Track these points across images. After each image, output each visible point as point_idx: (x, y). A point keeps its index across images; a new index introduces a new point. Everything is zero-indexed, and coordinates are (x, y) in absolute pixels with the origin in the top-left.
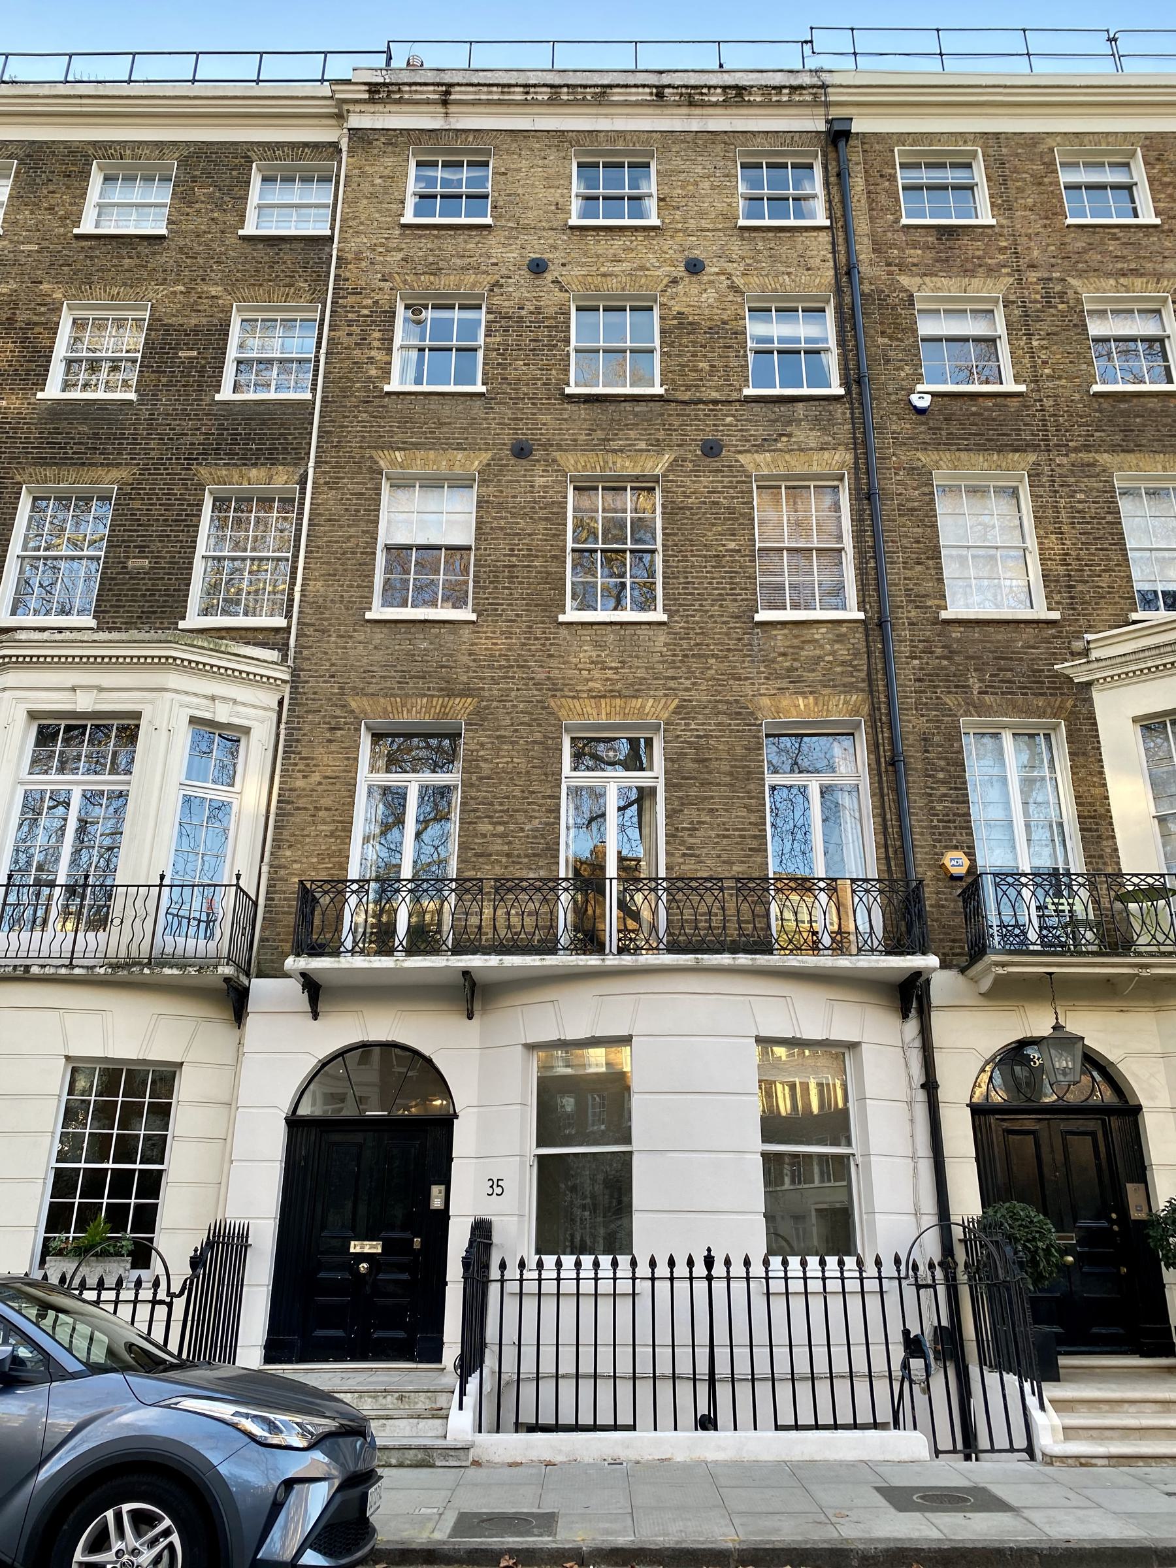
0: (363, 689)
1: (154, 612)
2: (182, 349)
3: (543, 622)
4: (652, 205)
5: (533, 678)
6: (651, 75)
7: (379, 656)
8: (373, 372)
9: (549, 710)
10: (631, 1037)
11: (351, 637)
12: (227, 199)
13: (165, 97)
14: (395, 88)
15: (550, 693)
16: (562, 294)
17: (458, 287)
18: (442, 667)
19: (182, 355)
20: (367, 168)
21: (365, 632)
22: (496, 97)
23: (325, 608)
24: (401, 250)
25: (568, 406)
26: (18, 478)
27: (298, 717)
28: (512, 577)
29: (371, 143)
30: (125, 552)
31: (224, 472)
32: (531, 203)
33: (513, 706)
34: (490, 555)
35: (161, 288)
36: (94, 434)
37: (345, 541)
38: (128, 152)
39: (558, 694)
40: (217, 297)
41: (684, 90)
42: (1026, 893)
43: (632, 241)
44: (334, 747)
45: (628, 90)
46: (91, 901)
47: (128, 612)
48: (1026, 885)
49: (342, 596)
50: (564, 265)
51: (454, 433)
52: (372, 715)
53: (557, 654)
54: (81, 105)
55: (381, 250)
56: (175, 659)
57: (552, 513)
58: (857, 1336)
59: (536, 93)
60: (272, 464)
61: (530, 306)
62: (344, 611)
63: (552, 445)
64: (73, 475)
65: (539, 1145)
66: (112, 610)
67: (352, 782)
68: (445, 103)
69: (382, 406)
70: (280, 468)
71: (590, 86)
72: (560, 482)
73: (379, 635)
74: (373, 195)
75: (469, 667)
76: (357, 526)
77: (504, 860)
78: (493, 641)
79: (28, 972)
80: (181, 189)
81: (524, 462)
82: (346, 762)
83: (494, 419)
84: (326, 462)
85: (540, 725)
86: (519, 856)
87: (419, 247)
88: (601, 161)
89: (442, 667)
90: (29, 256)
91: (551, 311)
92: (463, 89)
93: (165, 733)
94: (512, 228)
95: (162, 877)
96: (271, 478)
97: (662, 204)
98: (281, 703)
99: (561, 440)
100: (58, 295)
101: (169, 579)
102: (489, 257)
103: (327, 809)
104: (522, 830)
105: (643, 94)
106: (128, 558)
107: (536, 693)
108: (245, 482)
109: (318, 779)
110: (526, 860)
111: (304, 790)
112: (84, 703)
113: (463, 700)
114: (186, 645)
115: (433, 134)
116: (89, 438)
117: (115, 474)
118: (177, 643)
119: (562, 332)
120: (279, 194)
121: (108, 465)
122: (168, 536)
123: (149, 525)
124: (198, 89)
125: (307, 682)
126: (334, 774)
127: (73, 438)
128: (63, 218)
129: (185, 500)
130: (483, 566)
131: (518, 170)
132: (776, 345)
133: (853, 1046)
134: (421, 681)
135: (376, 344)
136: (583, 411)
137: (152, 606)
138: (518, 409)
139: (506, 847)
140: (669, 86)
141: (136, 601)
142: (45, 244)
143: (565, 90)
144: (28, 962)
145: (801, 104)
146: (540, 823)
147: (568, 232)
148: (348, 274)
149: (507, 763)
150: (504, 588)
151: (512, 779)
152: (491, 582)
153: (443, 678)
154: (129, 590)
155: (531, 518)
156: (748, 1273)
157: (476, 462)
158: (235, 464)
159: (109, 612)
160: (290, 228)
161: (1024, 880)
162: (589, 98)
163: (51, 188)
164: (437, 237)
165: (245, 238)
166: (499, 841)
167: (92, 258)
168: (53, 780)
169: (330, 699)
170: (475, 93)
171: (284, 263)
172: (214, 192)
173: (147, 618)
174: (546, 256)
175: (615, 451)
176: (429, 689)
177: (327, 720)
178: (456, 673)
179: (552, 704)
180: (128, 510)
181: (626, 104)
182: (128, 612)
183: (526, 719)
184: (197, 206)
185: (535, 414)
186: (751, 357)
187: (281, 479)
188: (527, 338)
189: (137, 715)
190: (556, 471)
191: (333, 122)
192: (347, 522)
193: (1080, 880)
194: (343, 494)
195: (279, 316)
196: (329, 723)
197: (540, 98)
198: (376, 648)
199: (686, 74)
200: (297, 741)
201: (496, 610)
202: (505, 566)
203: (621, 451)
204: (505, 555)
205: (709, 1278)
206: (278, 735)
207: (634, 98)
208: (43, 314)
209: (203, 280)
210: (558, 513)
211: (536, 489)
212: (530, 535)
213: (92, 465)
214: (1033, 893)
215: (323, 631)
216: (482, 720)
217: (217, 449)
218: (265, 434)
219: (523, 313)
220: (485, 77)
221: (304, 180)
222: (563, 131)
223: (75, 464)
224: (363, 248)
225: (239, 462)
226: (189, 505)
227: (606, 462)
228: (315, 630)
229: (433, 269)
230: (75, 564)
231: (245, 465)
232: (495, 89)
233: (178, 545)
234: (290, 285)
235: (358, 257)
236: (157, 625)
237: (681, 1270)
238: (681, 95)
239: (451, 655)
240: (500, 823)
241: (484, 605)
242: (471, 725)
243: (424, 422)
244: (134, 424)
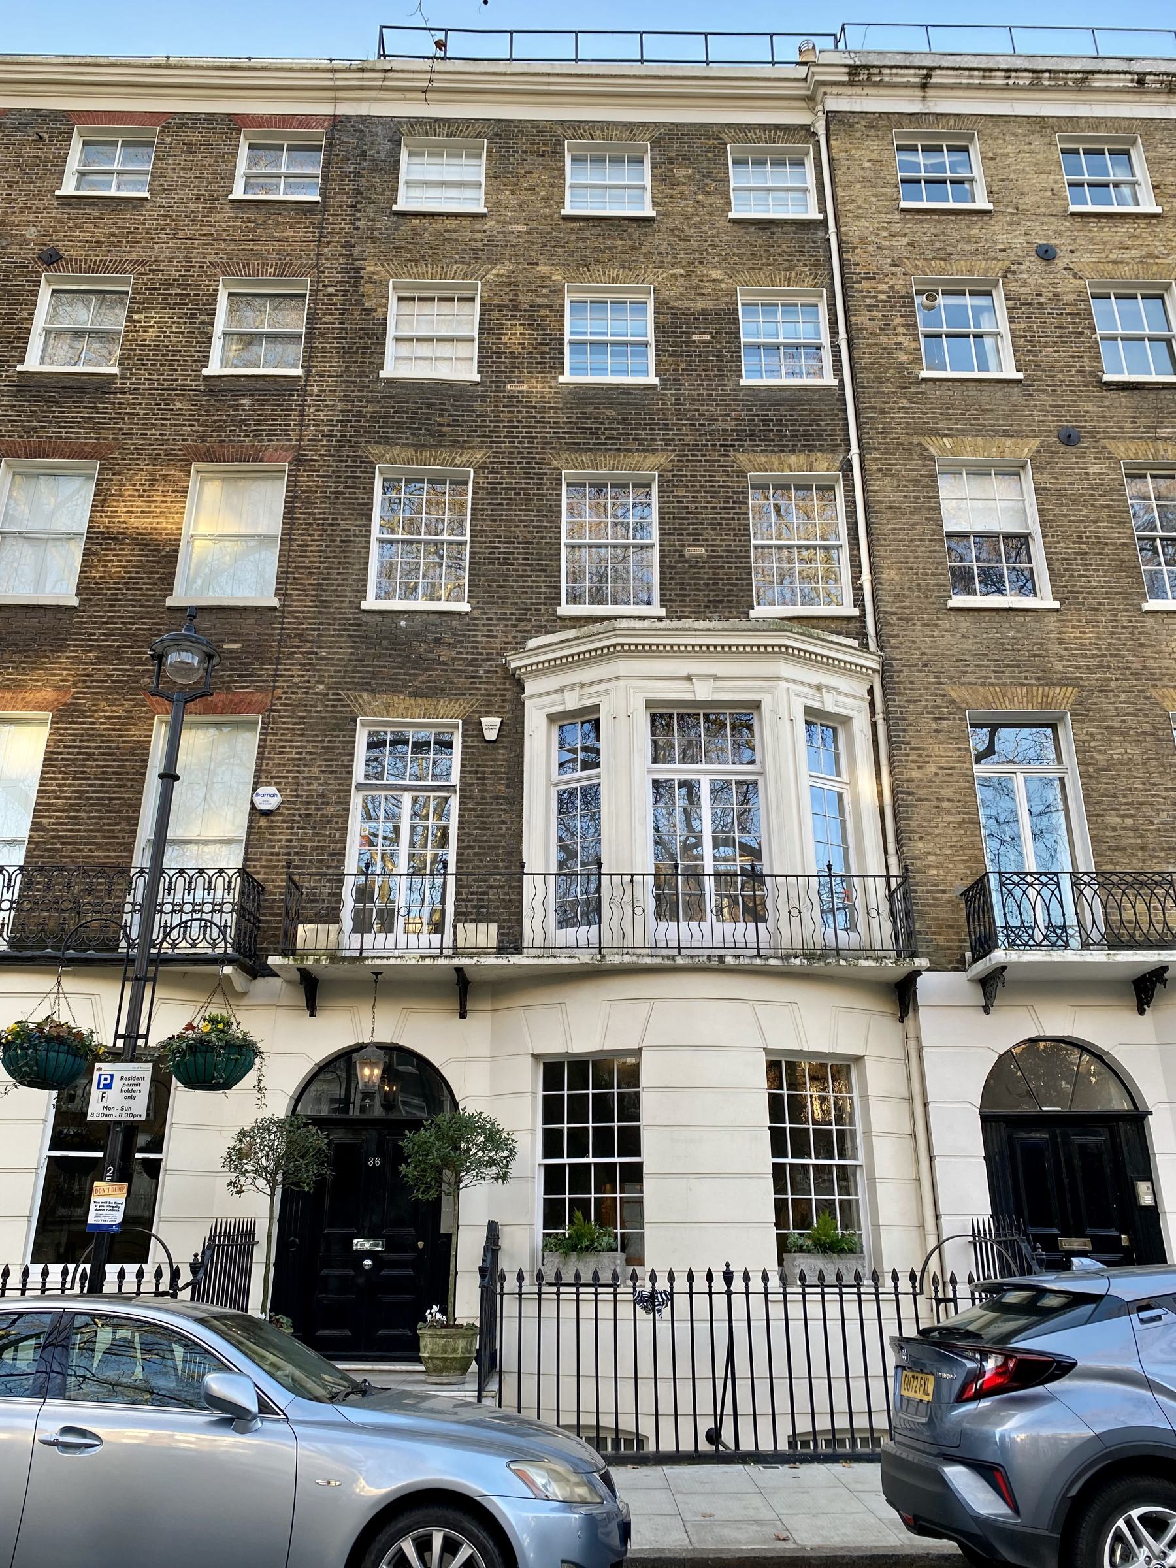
0: (959, 678)
1: (721, 601)
2: (694, 333)
3: (1127, 611)
4: (980, 190)
5: (1129, 668)
6: (1121, 62)
7: (968, 645)
8: (904, 358)
9: (1153, 701)
10: (640, 1049)
11: (936, 626)
12: (708, 181)
13: (635, 77)
14: (876, 71)
15: (1150, 683)
16: (1078, 281)
17: (971, 272)
18: (1035, 655)
19: (698, 339)
20: (853, 152)
21: (950, 620)
22: (977, 81)
23: (904, 595)
24: (905, 234)
25: (1108, 394)
26: (555, 464)
27: (900, 707)
28: (1086, 565)
29: (851, 126)
30: (679, 540)
31: (763, 459)
32: (1026, 189)
33: (1115, 696)
34: (1059, 543)
35: (661, 270)
36: (623, 419)
37: (900, 525)
38: (598, 132)
39: (1158, 683)
40: (719, 281)
41: (1165, 78)
42: (1032, 893)
43: (1135, 229)
44: (942, 737)
45: (1110, 76)
46: (748, 893)
47: (695, 601)
48: (1031, 884)
49: (918, 584)
50: (1072, 251)
51: (997, 420)
52: (974, 705)
53: (1147, 642)
54: (549, 83)
55: (885, 234)
56: (622, 645)
57: (1112, 500)
59: (1017, 78)
60: (810, 451)
61: (1047, 293)
62: (923, 600)
63: (1098, 432)
64: (610, 461)
66: (678, 599)
67: (970, 773)
68: (924, 86)
69: (921, 393)
70: (819, 454)
71: (1072, 72)
72: (1114, 469)
73: (964, 624)
74: (864, 180)
75: (1062, 656)
76: (919, 513)
77: (1140, 853)
78: (1082, 630)
79: (723, 962)
80: (660, 170)
81: (1073, 449)
82: (958, 753)
83: (1035, 406)
84: (875, 449)
85: (1146, 716)
86: (1154, 850)
87: (925, 231)
88: (1081, 147)
89: (1035, 655)
90: (519, 237)
91: (1070, 298)
92: (944, 72)
93: (788, 723)
94: (1012, 214)
95: (830, 867)
96: (811, 464)
97: (1157, 191)
98: (871, 691)
99: (1107, 427)
100: (557, 277)
101: (730, 568)
102: (996, 243)
103: (949, 800)
104: (1152, 823)
105: (1124, 80)
106: (683, 546)
107: (1135, 682)
108: (786, 468)
109: (934, 770)
110: (1162, 854)
111: (921, 780)
112: (703, 692)
113: (1064, 689)
114: (798, 633)
115: (913, 118)
116: (618, 423)
117: (652, 460)
118: (791, 631)
119: (1086, 319)
120: (590, 175)
121: (644, 451)
122: (719, 524)
123: (698, 513)
124: (714, 70)
125: (901, 671)
126: (949, 765)
127: (602, 423)
128: (548, 197)
129: (729, 487)
130: (1055, 554)
131: (1007, 155)
134: (1017, 670)
135: (901, 329)
136: (1123, 398)
137: (717, 595)
138: (1058, 396)
139: (1139, 841)
140: (1150, 73)
141: (700, 590)
142: (533, 224)
143: (1047, 75)
144: (722, 952)
145: (1017, 88)
146: (1169, 816)
147: (1069, 218)
148: (858, 259)
149: (1121, 754)
150: (1080, 576)
151: (1129, 770)
152: (1065, 570)
153: (1037, 667)
154: (690, 579)
155: (1092, 505)
157: (1027, 448)
158: (773, 451)
159: (675, 601)
160: (768, 211)
161: (1029, 879)
162: (1070, 83)
163: (527, 168)
164: (939, 222)
165: (734, 221)
166: (1131, 834)
167: (584, 240)
168: (676, 770)
169: (928, 689)
170: (956, 77)
171: (779, 246)
172: (693, 175)
173: (715, 607)
174: (1053, 242)
175: (1165, 439)
176: (1026, 678)
177: (930, 710)
178: (1049, 662)
179: (1154, 694)
180: (674, 497)
181: (1106, 90)
182: (695, 601)
183: (1131, 710)
184: (680, 188)
185: (1075, 401)
186: (922, 339)
187: (823, 466)
188: (1052, 324)
189: (757, 705)
190: (1109, 458)
191: (803, 104)
192: (908, 510)
193: (1086, 878)
194: (899, 481)
195: (779, 300)
196: (932, 713)
197: (1021, 83)
198: (963, 636)
199: (1155, 62)
200: (904, 731)
201: (1077, 598)
202: (1077, 554)
203: (1170, 439)
204: (1074, 543)
205: (729, 1293)
206: (874, 725)
207: (1115, 85)
208: (545, 296)
209: (701, 263)
210: (1119, 501)
211: (1092, 476)
212: (1095, 522)
213: (628, 450)
214: (1039, 893)
215: (908, 620)
216: (1089, 710)
217: (752, 435)
218: (797, 420)
219: (1042, 300)
220: (955, 61)
221: (594, 160)
222: (1043, 117)
223: (610, 450)
224: (867, 232)
225: (776, 449)
226: (734, 492)
227: (1157, 451)
228: (899, 619)
229: (942, 254)
230: (602, 550)
231: (782, 451)
232: (976, 73)
233: (732, 533)
234: (791, 269)
235: (863, 241)
236: (727, 614)
237: (700, 1284)
238: (1162, 82)
239: (1042, 644)
240: (1128, 816)
241: (1063, 592)
242: (1077, 715)
243: (975, 408)
244: (662, 409)
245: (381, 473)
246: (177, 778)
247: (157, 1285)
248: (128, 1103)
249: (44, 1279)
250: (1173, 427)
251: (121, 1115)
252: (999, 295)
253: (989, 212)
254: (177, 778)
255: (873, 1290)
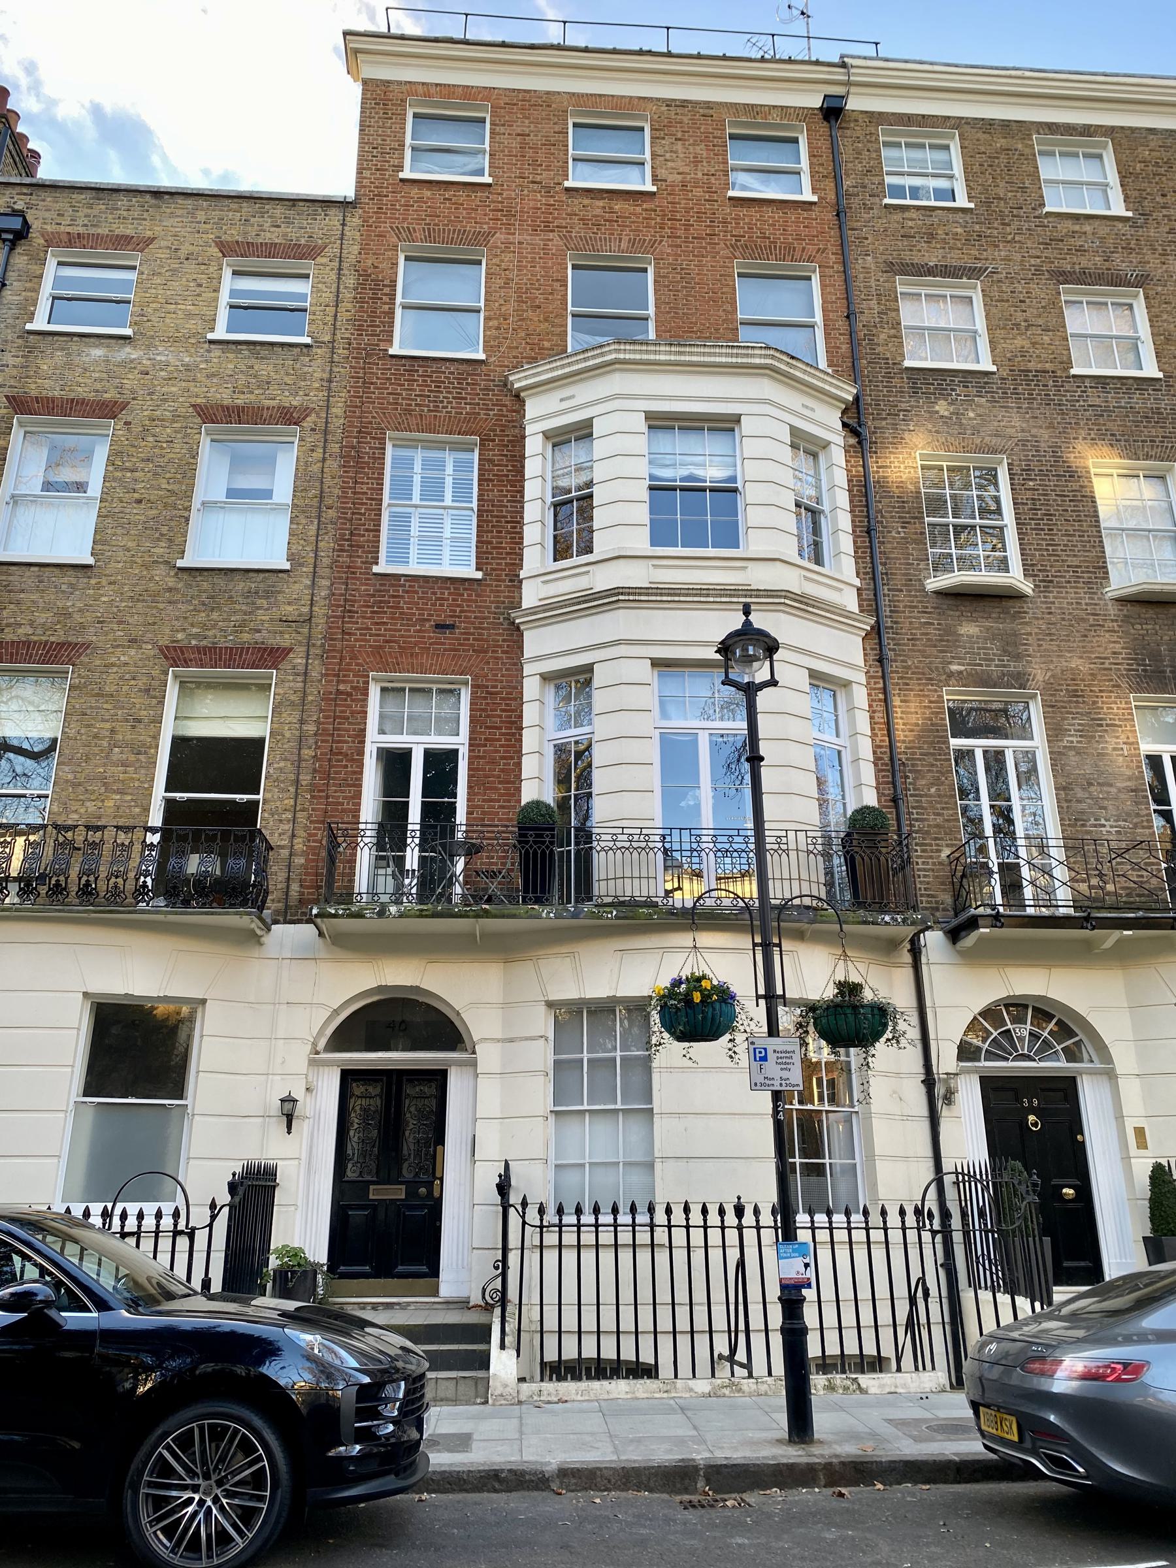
19: (1025, 322)
237: (714, 1219)
246: (762, 759)
247: (175, 1225)
248: (785, 1074)
249: (158, 1222)
251: (781, 1085)
254: (762, 759)
255: (864, 1225)
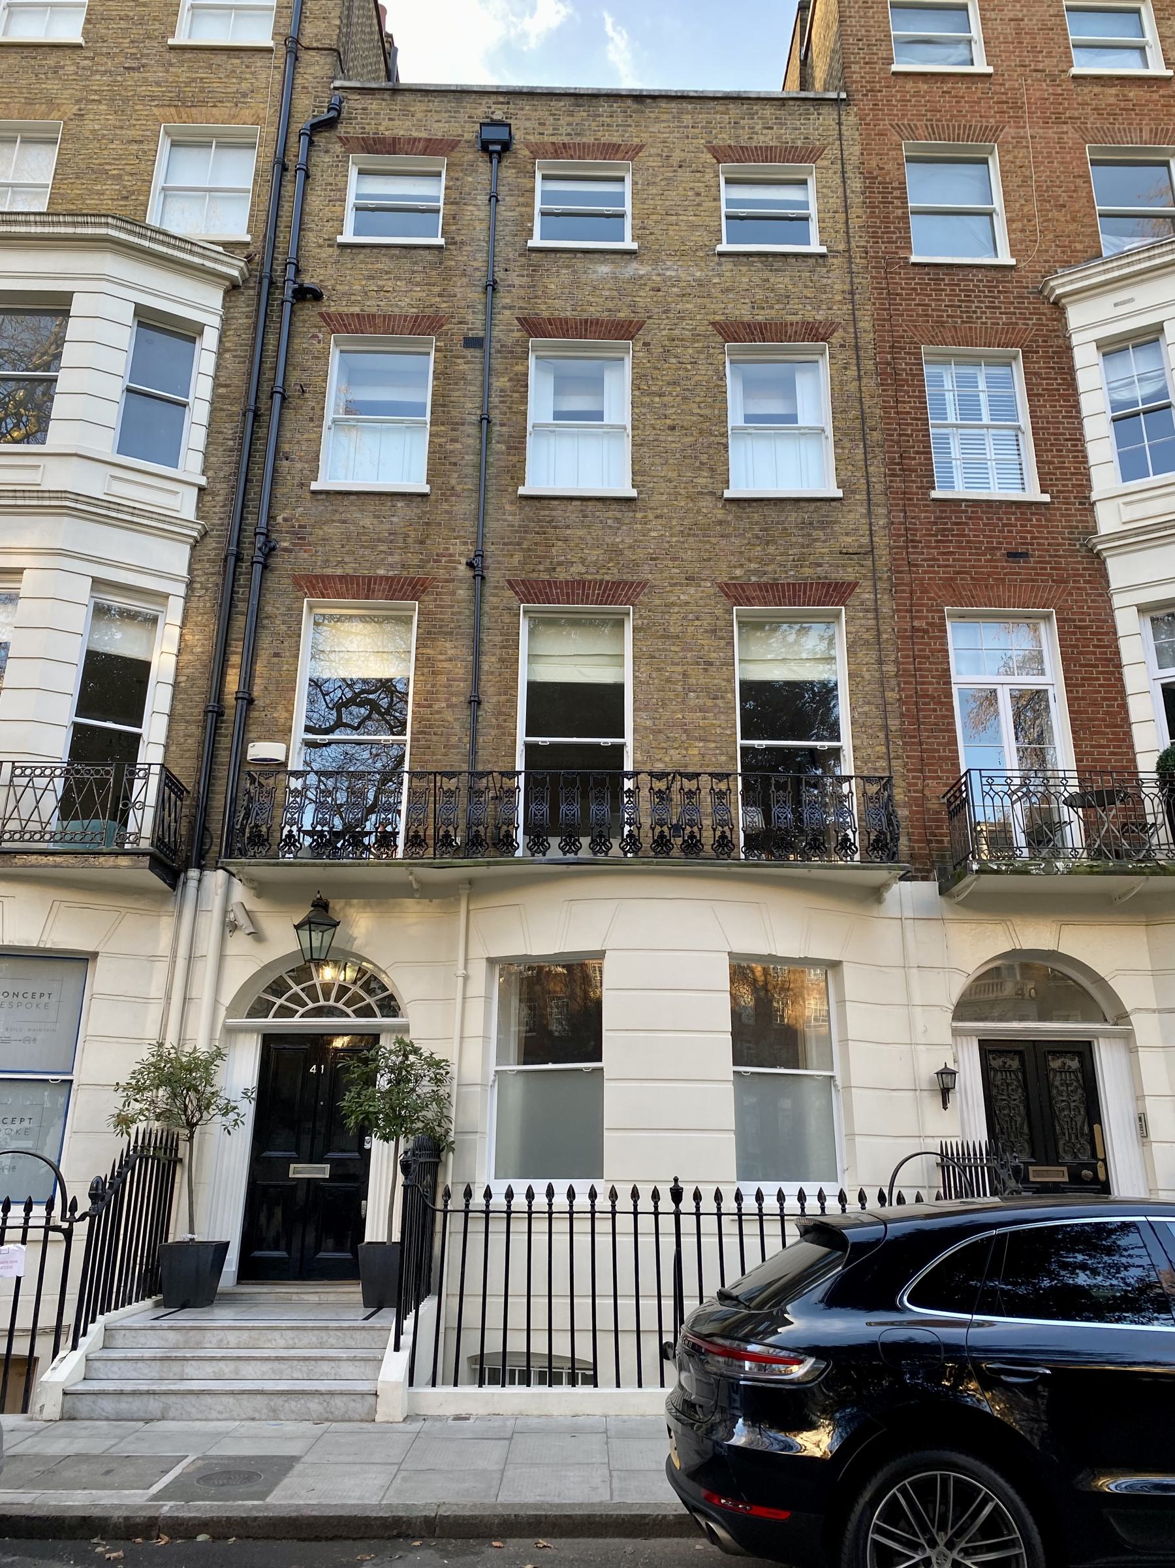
10: (604, 952)
58: (561, 1285)
65: (497, 1065)
132: (1141, 407)
133: (835, 965)
156: (635, 1206)
245: (167, 133)
250: (1172, 251)
252: (1018, 368)
253: (989, 75)
